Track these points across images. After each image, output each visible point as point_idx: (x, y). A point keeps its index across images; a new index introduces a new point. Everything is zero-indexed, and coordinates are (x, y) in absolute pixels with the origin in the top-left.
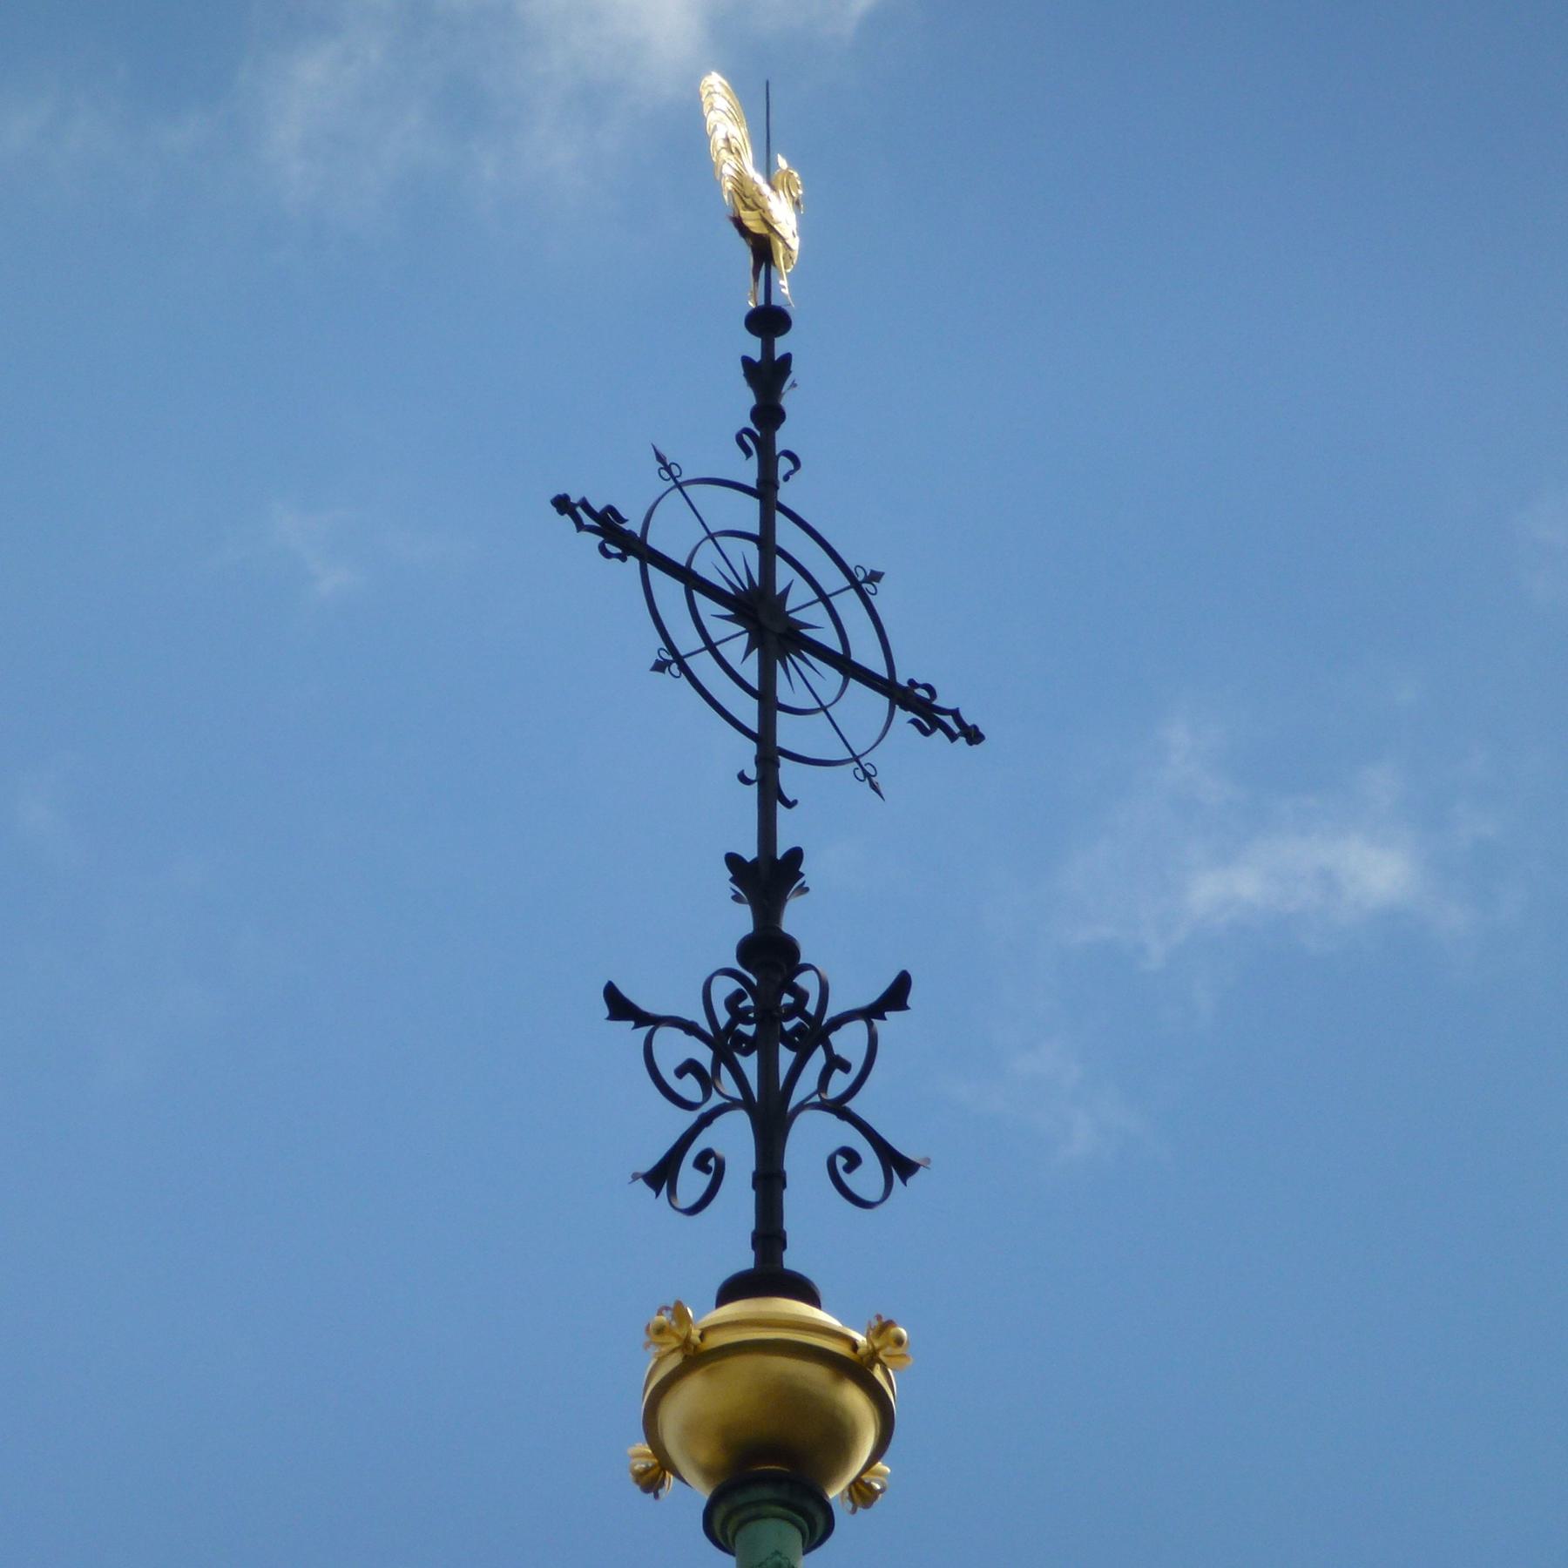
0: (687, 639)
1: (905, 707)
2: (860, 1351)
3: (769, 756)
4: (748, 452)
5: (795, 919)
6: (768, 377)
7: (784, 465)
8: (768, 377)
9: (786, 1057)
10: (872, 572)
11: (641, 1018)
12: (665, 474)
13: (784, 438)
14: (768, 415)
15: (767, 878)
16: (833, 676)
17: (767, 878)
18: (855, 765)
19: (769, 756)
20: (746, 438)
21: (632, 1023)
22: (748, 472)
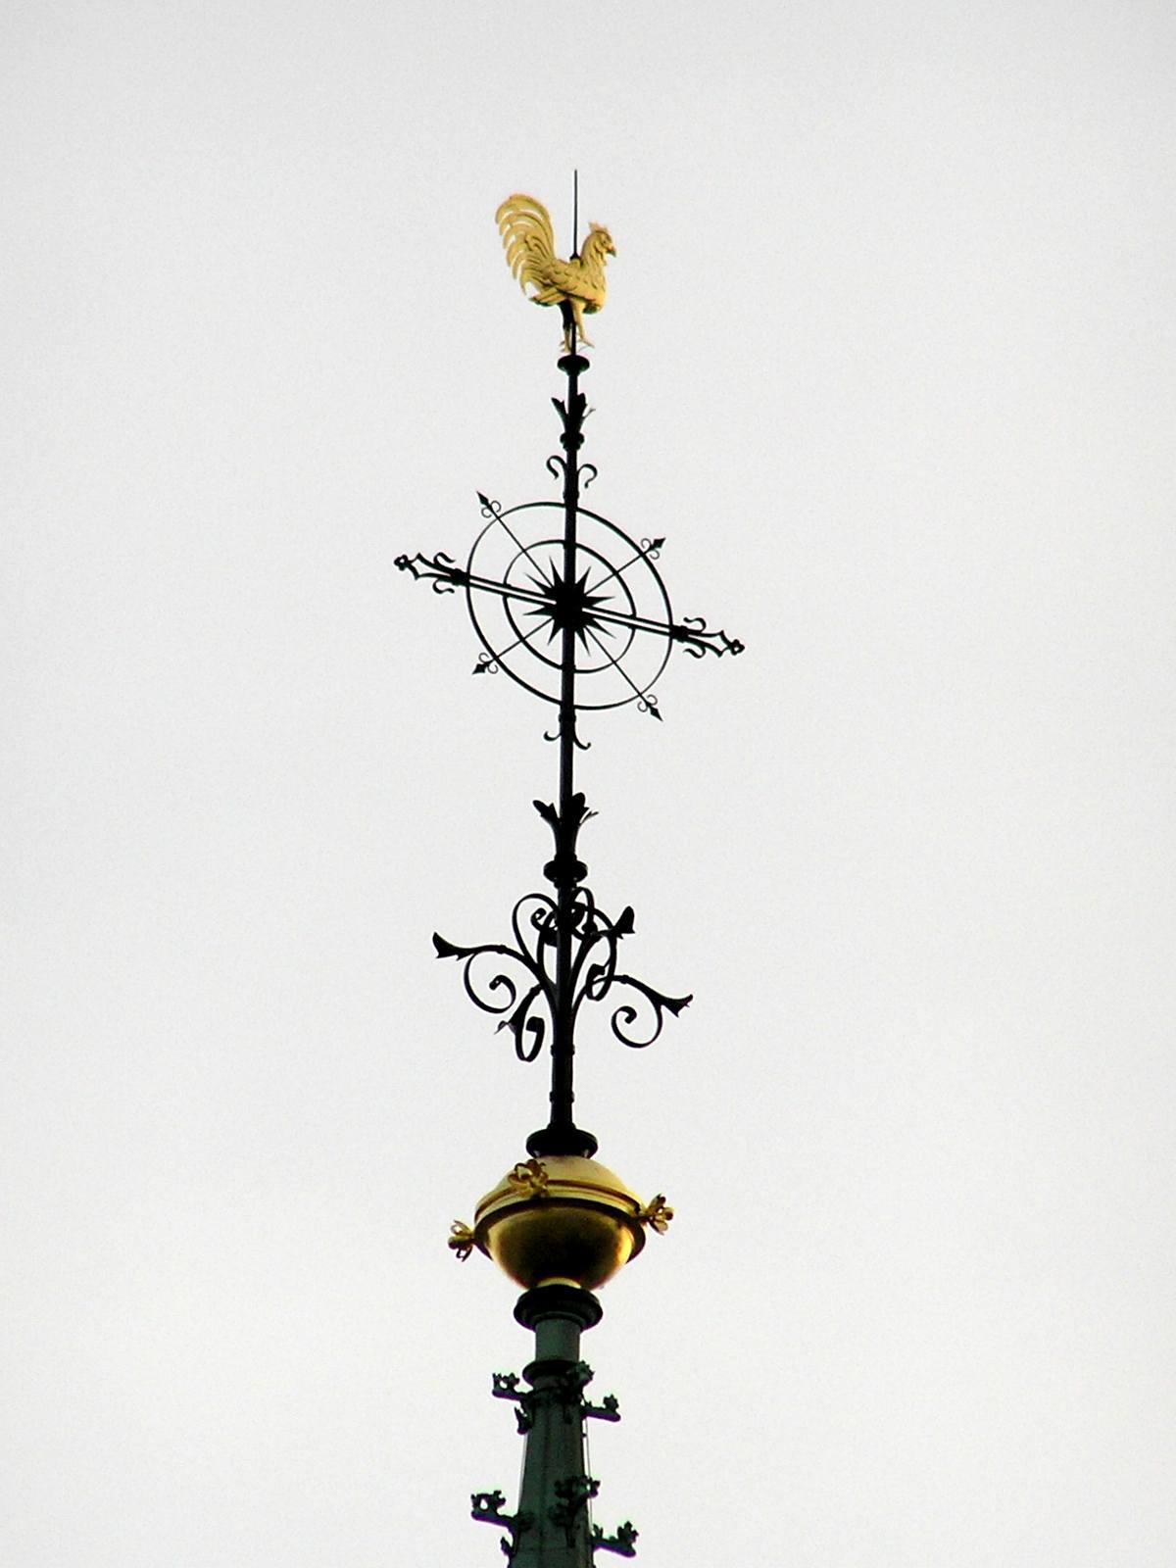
0: (501, 637)
1: (458, 571)
2: (641, 1212)
3: (568, 711)
4: (556, 474)
5: (585, 848)
6: (573, 411)
7: (584, 475)
8: (573, 411)
9: (576, 944)
10: (483, 671)
11: (462, 953)
12: (487, 512)
13: (583, 456)
14: (572, 439)
15: (567, 816)
16: (516, 580)
17: (567, 816)
18: (639, 699)
19: (568, 711)
20: (555, 463)
21: (456, 957)
22: (557, 489)
